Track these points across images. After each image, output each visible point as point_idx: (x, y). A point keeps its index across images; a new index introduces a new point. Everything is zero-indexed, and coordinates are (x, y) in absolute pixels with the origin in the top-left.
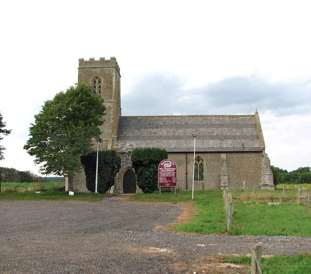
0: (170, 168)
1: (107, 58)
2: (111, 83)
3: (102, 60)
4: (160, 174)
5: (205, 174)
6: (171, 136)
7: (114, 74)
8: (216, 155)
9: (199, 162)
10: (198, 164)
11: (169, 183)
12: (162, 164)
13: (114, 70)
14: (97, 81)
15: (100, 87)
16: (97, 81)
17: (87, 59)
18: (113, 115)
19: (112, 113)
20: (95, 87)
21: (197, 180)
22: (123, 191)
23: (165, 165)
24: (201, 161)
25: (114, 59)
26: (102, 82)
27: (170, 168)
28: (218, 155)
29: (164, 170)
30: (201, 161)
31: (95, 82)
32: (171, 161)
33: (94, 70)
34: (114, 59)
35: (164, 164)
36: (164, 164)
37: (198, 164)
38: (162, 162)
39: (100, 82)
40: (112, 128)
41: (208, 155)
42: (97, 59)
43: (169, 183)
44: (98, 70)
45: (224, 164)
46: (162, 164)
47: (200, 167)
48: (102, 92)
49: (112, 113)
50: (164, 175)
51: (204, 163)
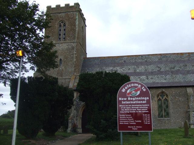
0: (138, 96)
1: (72, 4)
2: (75, 26)
3: (67, 6)
4: (120, 110)
5: (171, 111)
6: (132, 73)
7: (77, 17)
8: (181, 89)
9: (163, 98)
10: (163, 100)
11: (138, 124)
12: (124, 90)
13: (77, 14)
14: (62, 24)
15: (65, 30)
16: (62, 24)
17: (53, 6)
18: (76, 54)
19: (75, 52)
20: (60, 30)
21: (162, 117)
22: (81, 130)
23: (128, 91)
24: (165, 96)
25: (77, 5)
26: (67, 25)
27: (138, 96)
28: (184, 89)
29: (127, 100)
30: (165, 96)
31: (60, 26)
32: (139, 84)
33: (59, 15)
34: (77, 5)
35: (126, 90)
36: (126, 90)
37: (163, 100)
38: (124, 87)
39: (65, 25)
40: (75, 67)
41: (173, 90)
42: (63, 5)
43: (138, 124)
44: (63, 15)
45: (75, 115)
46: (124, 90)
47: (165, 103)
48: (66, 34)
49: (75, 52)
50: (127, 110)
51: (169, 98)
